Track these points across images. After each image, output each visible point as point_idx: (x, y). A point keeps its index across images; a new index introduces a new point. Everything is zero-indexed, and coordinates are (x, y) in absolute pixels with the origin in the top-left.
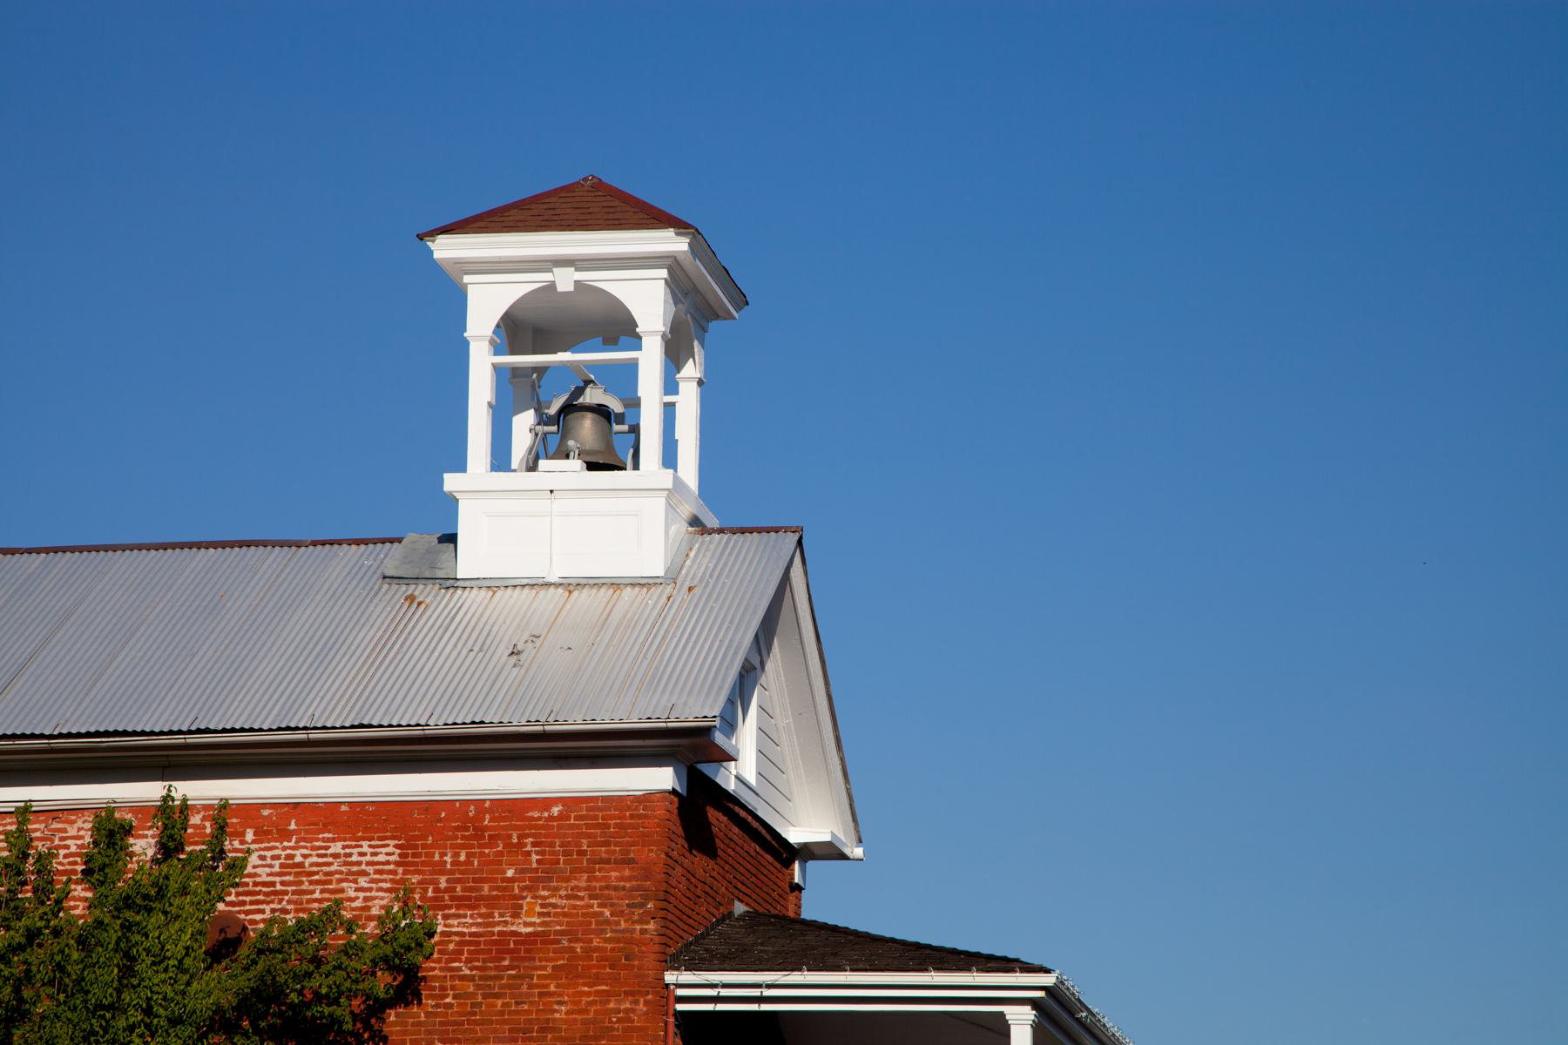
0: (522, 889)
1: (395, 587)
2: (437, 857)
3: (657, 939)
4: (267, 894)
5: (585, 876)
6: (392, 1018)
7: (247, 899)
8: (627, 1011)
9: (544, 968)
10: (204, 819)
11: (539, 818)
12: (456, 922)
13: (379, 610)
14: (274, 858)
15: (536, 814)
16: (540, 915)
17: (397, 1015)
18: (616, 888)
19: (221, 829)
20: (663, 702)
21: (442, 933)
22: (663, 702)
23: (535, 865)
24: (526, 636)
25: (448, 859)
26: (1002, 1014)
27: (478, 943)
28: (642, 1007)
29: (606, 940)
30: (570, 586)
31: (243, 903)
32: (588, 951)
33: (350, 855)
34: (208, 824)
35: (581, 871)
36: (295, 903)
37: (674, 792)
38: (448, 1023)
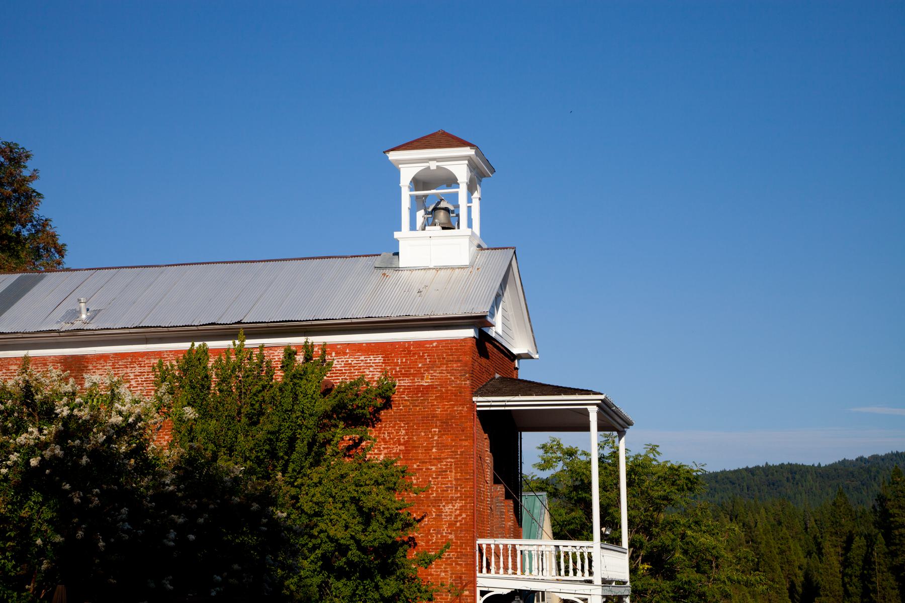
28: (465, 409)
30: (438, 269)
32: (447, 391)
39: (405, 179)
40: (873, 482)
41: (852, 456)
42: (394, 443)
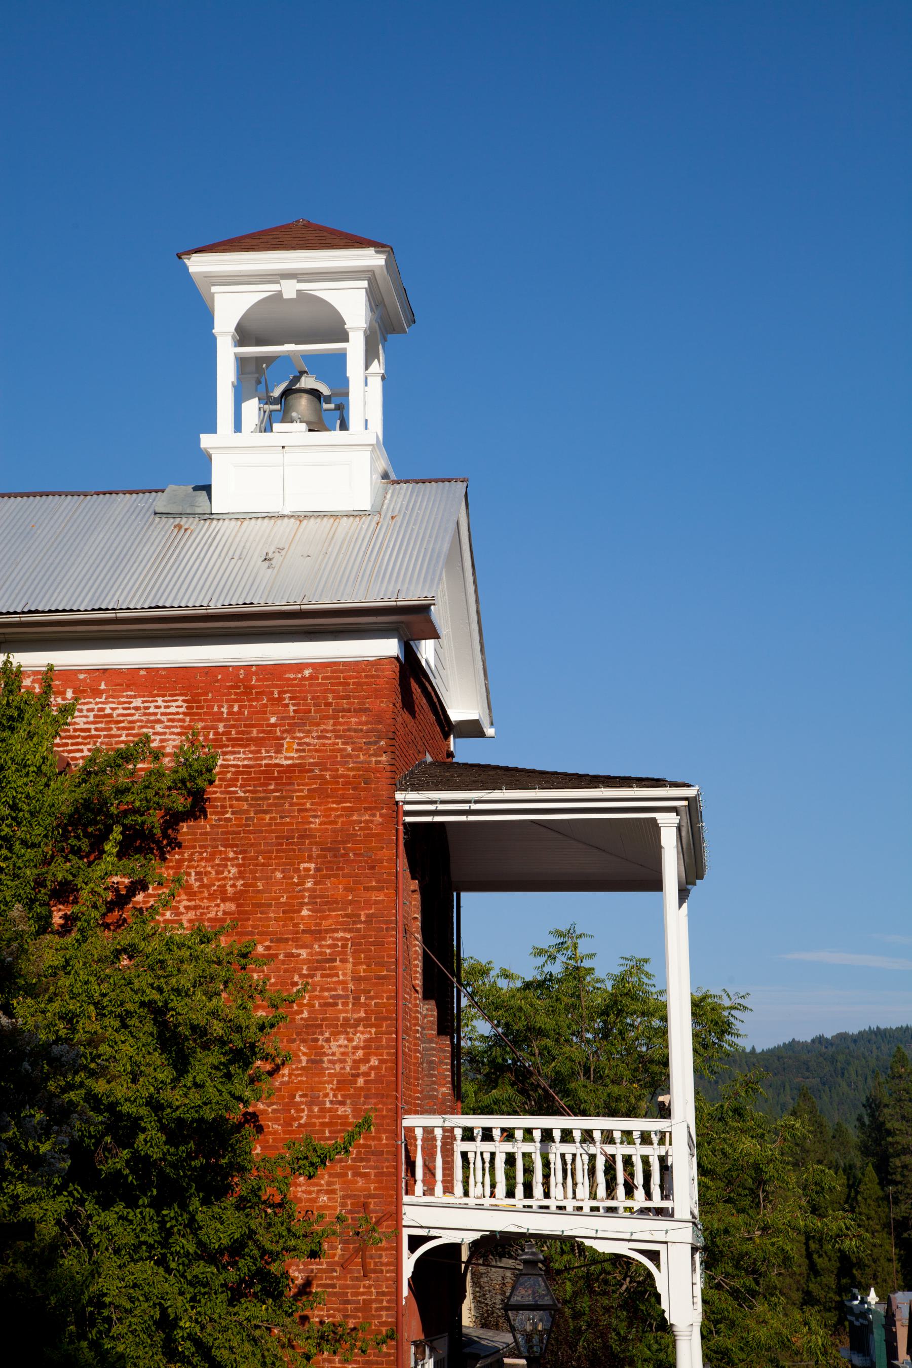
0: (282, 732)
1: (164, 520)
2: (216, 709)
3: (388, 768)
4: (84, 738)
5: (331, 722)
6: (185, 830)
7: (69, 741)
8: (366, 822)
9: (302, 791)
10: (33, 681)
11: (295, 679)
12: (232, 757)
13: (155, 534)
14: (88, 710)
15: (292, 676)
16: (297, 751)
17: (188, 827)
18: (355, 731)
19: (48, 689)
20: (391, 589)
21: (222, 766)
22: (391, 589)
23: (292, 714)
24: (273, 549)
25: (225, 710)
26: (654, 820)
27: (249, 773)
28: (378, 819)
29: (349, 769)
30: (301, 517)
31: (66, 745)
32: (335, 778)
33: (148, 708)
34: (37, 685)
35: (328, 717)
36: (107, 744)
37: (397, 658)
38: (227, 833)
39: (225, 323)
40: (839, 1079)
41: (806, 1036)
42: (212, 897)
